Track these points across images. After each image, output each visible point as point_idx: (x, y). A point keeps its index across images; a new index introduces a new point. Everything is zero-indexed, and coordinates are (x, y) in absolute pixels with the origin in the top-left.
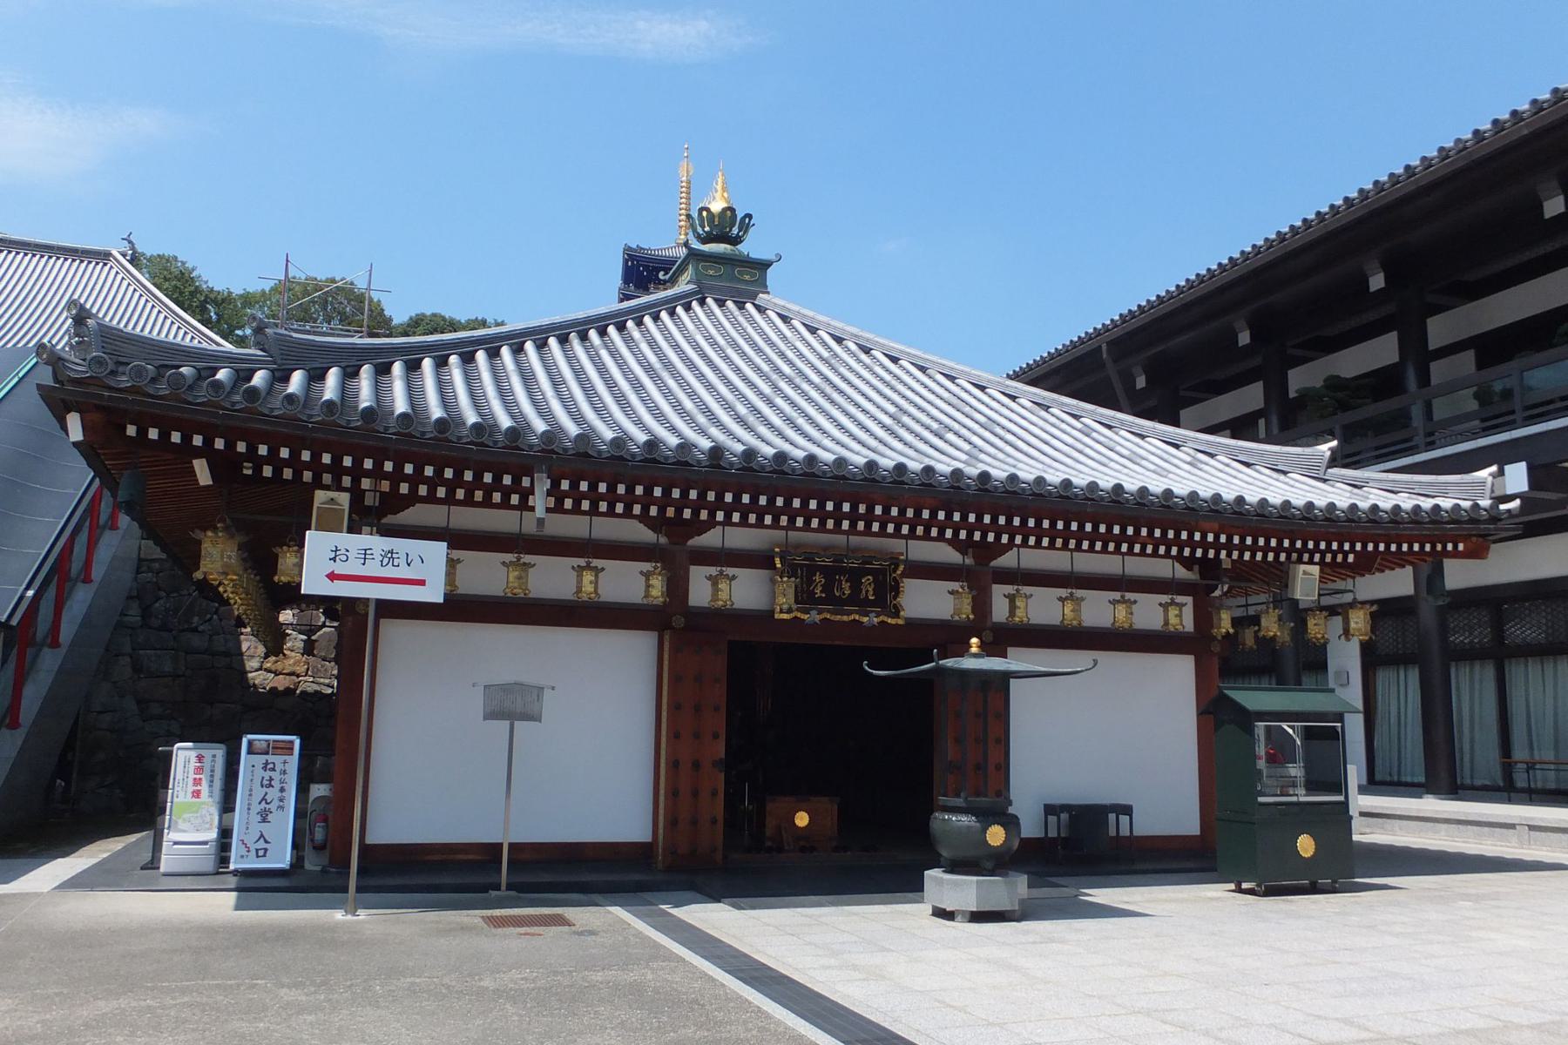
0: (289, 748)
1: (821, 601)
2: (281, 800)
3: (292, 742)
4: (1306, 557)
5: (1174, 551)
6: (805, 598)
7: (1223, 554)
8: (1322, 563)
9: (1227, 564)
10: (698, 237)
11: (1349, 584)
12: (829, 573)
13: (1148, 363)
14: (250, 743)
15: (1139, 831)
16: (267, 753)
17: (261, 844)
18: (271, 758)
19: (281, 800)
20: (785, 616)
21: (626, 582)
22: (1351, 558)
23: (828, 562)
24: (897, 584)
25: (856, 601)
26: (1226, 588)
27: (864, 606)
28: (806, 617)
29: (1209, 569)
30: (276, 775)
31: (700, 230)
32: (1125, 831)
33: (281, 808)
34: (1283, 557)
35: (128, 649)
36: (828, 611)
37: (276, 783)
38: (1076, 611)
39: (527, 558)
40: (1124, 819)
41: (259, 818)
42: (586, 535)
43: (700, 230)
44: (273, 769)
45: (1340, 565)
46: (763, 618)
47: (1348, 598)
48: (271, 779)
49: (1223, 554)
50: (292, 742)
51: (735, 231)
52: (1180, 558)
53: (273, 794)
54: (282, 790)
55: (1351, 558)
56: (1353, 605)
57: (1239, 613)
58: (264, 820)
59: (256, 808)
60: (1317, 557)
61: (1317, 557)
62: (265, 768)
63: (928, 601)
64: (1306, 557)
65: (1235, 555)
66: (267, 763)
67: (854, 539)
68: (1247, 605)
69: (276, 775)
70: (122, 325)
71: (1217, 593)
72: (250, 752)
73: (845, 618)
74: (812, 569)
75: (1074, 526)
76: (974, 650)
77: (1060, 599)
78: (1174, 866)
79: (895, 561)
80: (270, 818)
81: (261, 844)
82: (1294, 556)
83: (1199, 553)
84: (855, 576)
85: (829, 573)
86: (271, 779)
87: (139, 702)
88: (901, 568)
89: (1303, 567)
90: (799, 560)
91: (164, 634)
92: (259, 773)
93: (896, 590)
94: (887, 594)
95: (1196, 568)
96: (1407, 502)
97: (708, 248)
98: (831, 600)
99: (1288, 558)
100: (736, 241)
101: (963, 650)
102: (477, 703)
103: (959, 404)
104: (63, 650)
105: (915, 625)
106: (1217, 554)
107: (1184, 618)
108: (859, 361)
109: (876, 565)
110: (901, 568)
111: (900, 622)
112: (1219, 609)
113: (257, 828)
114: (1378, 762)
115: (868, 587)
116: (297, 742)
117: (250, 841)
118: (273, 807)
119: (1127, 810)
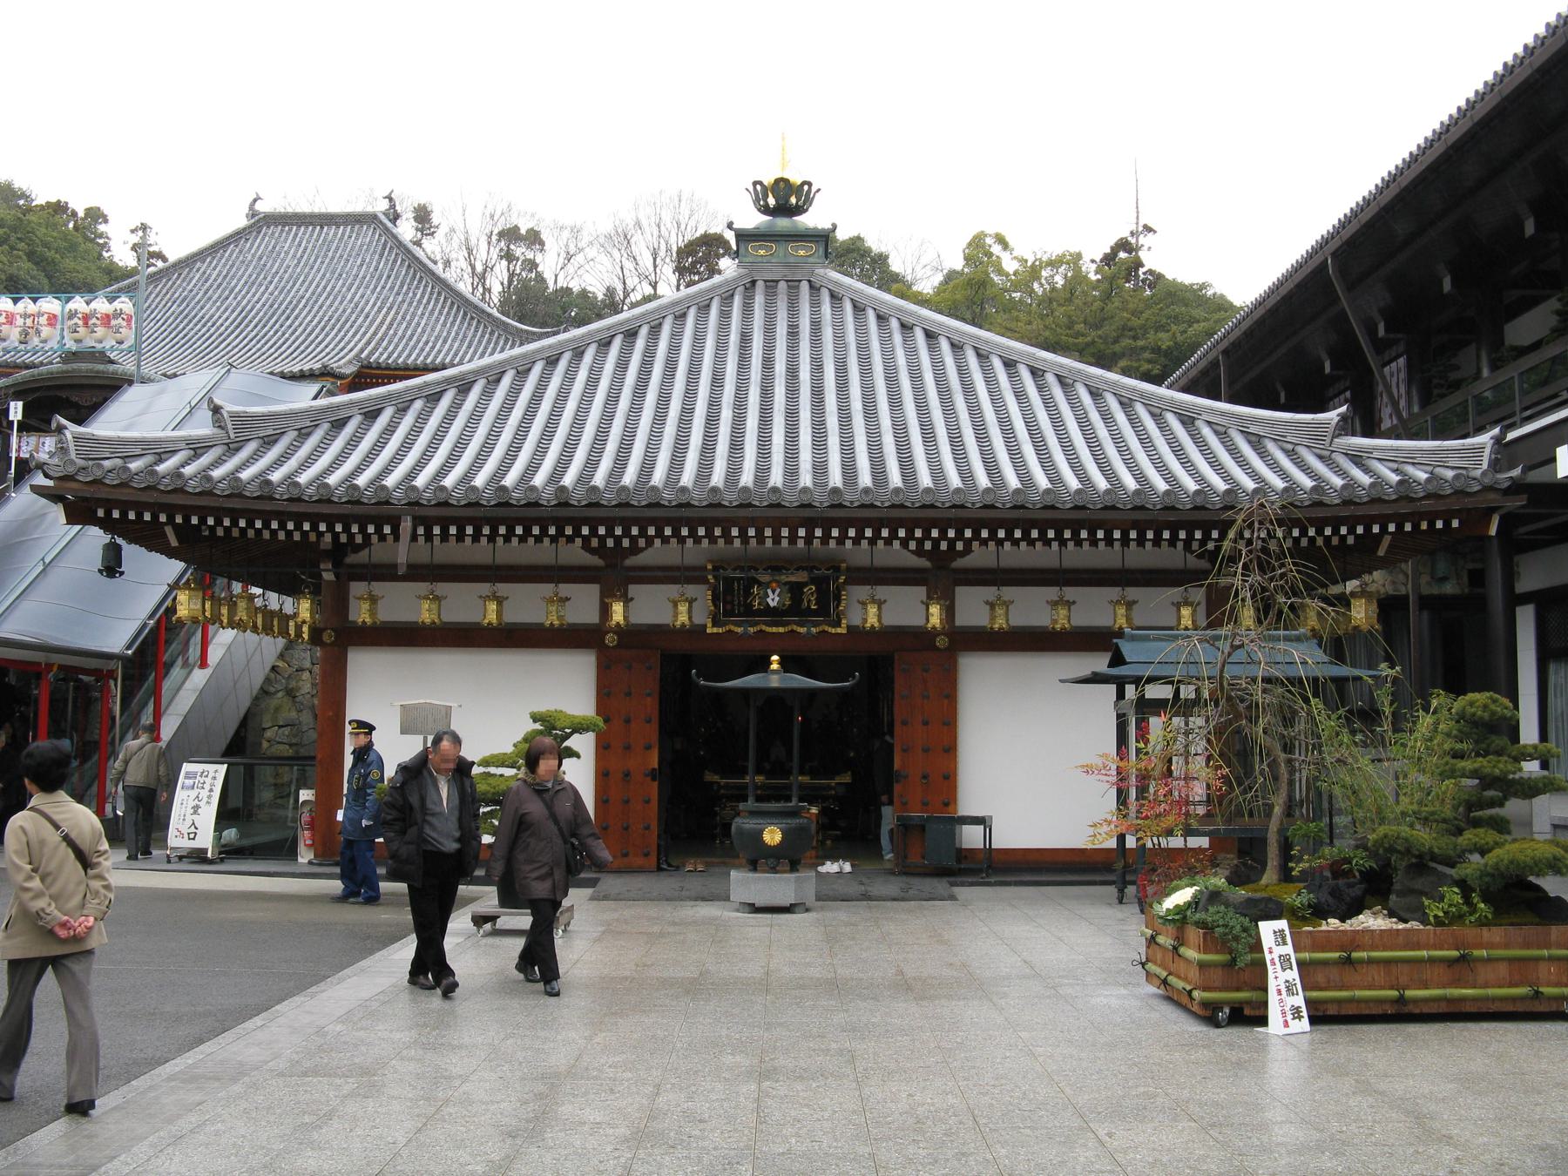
28: (802, 630)
73: (781, 630)
76: (775, 666)
78: (1098, 878)
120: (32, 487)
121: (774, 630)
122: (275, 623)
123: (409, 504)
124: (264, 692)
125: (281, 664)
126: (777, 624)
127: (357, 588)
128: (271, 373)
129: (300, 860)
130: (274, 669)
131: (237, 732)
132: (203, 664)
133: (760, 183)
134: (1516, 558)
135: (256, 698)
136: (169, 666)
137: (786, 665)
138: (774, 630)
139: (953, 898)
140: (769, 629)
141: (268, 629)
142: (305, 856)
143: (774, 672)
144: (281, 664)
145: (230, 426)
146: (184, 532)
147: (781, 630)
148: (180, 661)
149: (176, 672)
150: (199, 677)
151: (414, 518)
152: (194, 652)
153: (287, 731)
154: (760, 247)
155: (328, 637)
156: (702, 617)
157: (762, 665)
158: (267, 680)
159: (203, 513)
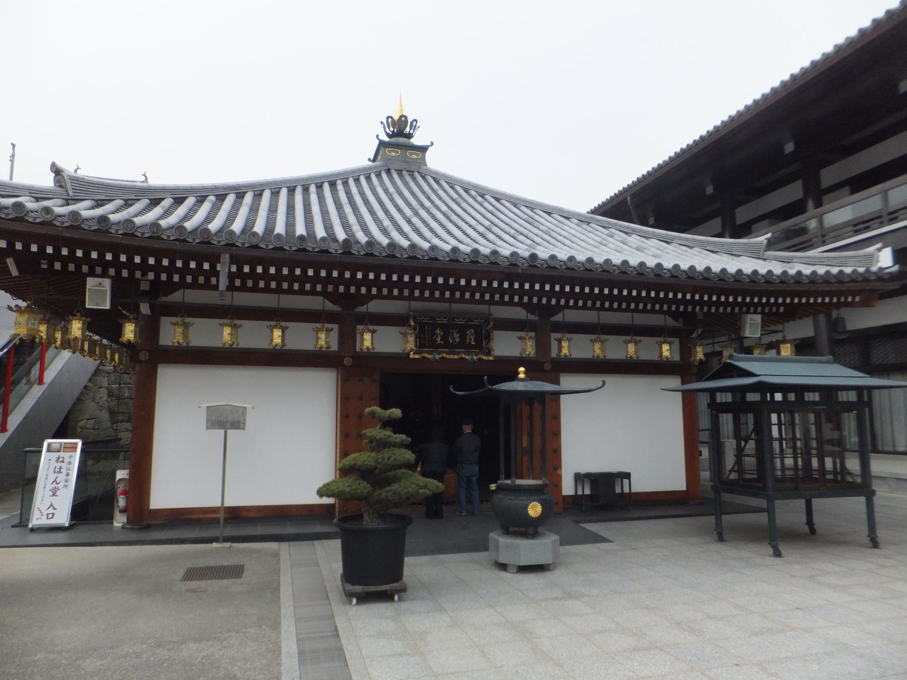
0: (73, 447)
1: (440, 346)
2: (66, 481)
3: (76, 444)
4: (752, 309)
5: (665, 307)
6: (421, 345)
7: (698, 309)
8: (762, 313)
9: (700, 317)
10: (388, 135)
11: (780, 327)
12: (446, 329)
13: (658, 200)
14: (49, 445)
15: (634, 489)
16: (59, 451)
17: (51, 510)
18: (61, 454)
19: (66, 481)
20: (417, 356)
21: (325, 339)
22: (782, 309)
23: (445, 321)
24: (489, 333)
25: (463, 345)
26: (700, 332)
27: (468, 347)
28: (467, 357)
29: (689, 319)
30: (64, 465)
31: (387, 130)
32: (626, 490)
33: (66, 486)
34: (737, 310)
35: (106, 384)
36: (445, 352)
37: (64, 471)
38: (185, 335)
39: (188, 320)
40: (626, 481)
41: (51, 493)
42: (276, 306)
43: (387, 130)
44: (63, 462)
45: (298, 264)
46: (403, 357)
47: (779, 337)
48: (61, 468)
49: (698, 309)
50: (76, 444)
51: (408, 129)
52: (669, 312)
53: (61, 477)
54: (67, 475)
55: (782, 309)
56: (784, 341)
57: (709, 349)
58: (54, 495)
59: (50, 486)
60: (759, 309)
61: (759, 309)
62: (57, 461)
63: (506, 345)
64: (752, 309)
65: (706, 309)
66: (59, 458)
67: (456, 307)
68: (713, 343)
69: (64, 465)
70: (280, 229)
71: (695, 335)
72: (49, 450)
73: (456, 357)
74: (435, 326)
75: (516, 286)
76: (522, 376)
77: (591, 341)
78: (653, 514)
79: (487, 318)
80: (58, 493)
81: (51, 510)
82: (744, 309)
83: (682, 308)
84: (462, 330)
85: (446, 329)
86: (61, 468)
87: (111, 413)
88: (492, 324)
89: (750, 316)
90: (426, 320)
91: (126, 376)
92: (54, 464)
93: (489, 338)
94: (483, 341)
95: (681, 320)
96: (778, 269)
97: (393, 140)
98: (447, 345)
99: (740, 310)
100: (409, 136)
101: (514, 377)
102: (202, 418)
103: (531, 222)
104: (45, 386)
105: (500, 360)
106: (694, 309)
107: (325, 339)
108: (476, 200)
109: (476, 322)
110: (492, 324)
111: (491, 358)
112: (696, 345)
113: (49, 499)
114: (83, 541)
115: (471, 339)
116: (79, 443)
117: (44, 508)
118: (60, 486)
119: (627, 476)
120: (120, 511)
121: (452, 356)
122: (97, 349)
123: (227, 245)
124: (79, 401)
125: (89, 384)
126: (454, 354)
127: (166, 323)
128: (13, 527)
129: (115, 524)
130: (85, 387)
131: (62, 423)
132: (41, 381)
133: (391, 117)
134: (676, 341)
135: (74, 404)
136: (16, 383)
137: (530, 376)
138: (452, 356)
139: (597, 539)
140: (448, 357)
141: (91, 353)
142: (119, 520)
143: (522, 380)
144: (89, 384)
145: (69, 186)
146: (26, 261)
147: (456, 357)
148: (24, 381)
149: (22, 385)
150: (37, 392)
151: (231, 257)
152: (35, 372)
153: (92, 421)
154: (393, 151)
155: (143, 356)
156: (411, 345)
157: (514, 377)
158: (82, 393)
159: (42, 241)
